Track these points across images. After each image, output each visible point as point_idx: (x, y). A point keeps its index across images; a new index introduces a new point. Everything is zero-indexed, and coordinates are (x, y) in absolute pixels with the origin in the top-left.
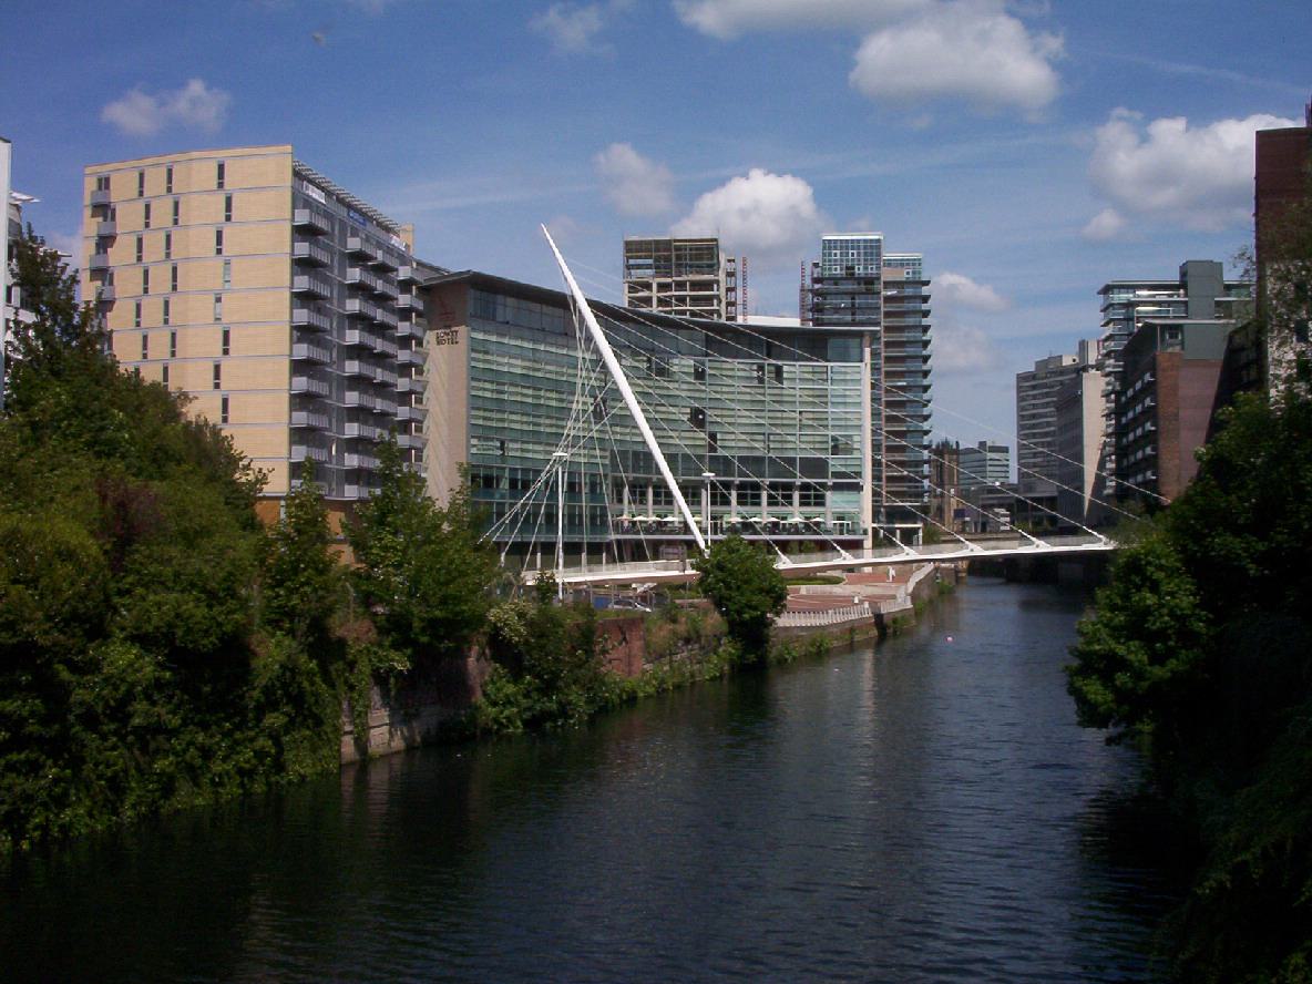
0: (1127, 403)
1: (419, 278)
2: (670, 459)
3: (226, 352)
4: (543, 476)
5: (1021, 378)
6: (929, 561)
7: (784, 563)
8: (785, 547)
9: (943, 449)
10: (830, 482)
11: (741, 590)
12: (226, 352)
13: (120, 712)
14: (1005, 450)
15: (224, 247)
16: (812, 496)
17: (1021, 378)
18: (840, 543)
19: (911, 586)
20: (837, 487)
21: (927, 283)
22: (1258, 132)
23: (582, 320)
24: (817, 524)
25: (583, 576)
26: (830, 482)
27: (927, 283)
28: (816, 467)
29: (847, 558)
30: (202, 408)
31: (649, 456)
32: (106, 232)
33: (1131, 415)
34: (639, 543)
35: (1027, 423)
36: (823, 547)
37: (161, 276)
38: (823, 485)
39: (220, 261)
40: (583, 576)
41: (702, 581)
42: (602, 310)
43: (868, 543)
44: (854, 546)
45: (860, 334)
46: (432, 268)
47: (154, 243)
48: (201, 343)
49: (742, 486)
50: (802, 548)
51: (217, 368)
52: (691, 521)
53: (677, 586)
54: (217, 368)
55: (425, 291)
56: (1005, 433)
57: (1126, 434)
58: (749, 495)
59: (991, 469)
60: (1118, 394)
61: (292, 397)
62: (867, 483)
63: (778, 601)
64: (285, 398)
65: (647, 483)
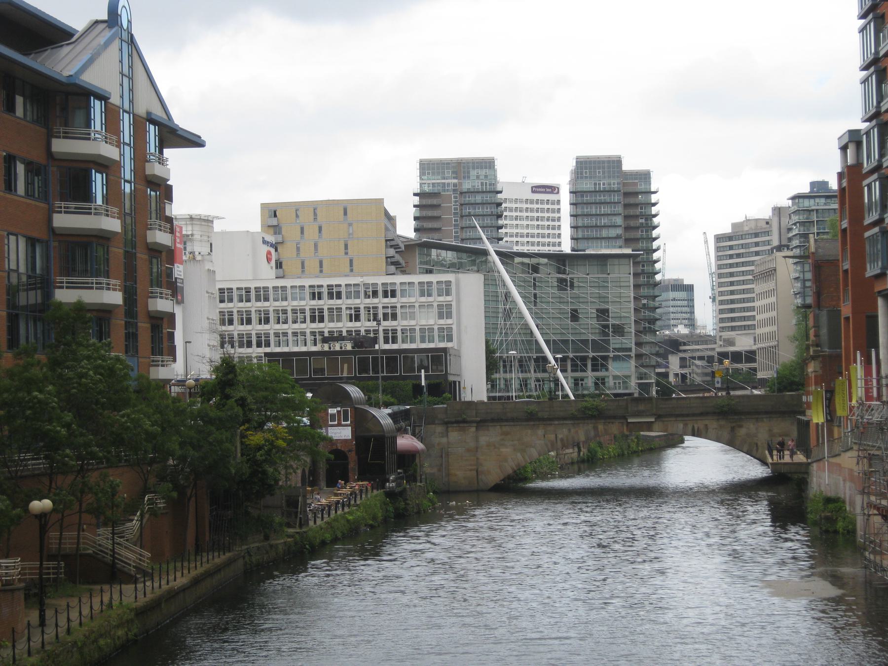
5: (719, 238)
10: (611, 355)
20: (616, 358)
22: (264, 206)
26: (611, 355)
38: (605, 358)
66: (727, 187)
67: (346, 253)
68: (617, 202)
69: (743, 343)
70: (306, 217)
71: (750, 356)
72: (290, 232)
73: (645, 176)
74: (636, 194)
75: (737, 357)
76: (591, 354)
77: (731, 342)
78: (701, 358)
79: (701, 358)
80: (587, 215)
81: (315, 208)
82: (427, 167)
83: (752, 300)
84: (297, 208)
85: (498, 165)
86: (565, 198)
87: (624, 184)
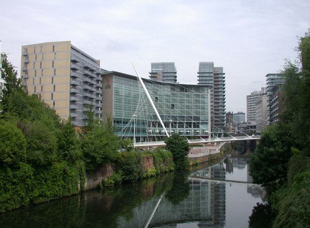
0: (272, 103)
1: (101, 73)
2: (162, 117)
3: (54, 90)
4: (131, 121)
5: (248, 96)
6: (224, 141)
7: (189, 142)
8: (190, 138)
9: (229, 114)
11: (177, 148)
12: (54, 90)
13: (23, 181)
14: (244, 114)
15: (55, 49)
16: (196, 126)
17: (248, 96)
18: (202, 137)
19: (220, 147)
20: (202, 123)
21: (224, 74)
23: (140, 83)
24: (197, 132)
25: (140, 145)
27: (224, 74)
28: (197, 118)
29: (204, 141)
30: (48, 102)
31: (156, 116)
32: (27, 61)
33: (273, 106)
34: (154, 137)
35: (249, 107)
36: (199, 138)
37: (39, 72)
38: (199, 123)
39: (53, 54)
40: (140, 145)
41: (167, 146)
42: (143, 79)
43: (210, 137)
44: (206, 137)
45: (208, 86)
46: (104, 70)
47: (38, 64)
48: (48, 88)
49: (179, 123)
50: (195, 138)
51: (52, 94)
52: (166, 131)
53: (162, 147)
54: (52, 94)
55: (103, 76)
56: (244, 109)
57: (272, 110)
58: (181, 125)
59: (211, 82)
60: (271, 100)
61: (70, 109)
62: (210, 123)
63: (187, 149)
64: (68, 110)
65: (156, 122)
66: (250, 71)
67: (53, 66)
68: (213, 80)
69: (253, 123)
70: (38, 50)
71: (255, 127)
72: (31, 58)
73: (221, 69)
74: (218, 74)
75: (251, 127)
76: (193, 122)
77: (250, 123)
78: (243, 128)
79: (243, 128)
80: (203, 80)
81: (41, 46)
82: (154, 65)
83: (255, 110)
84: (35, 47)
85: (176, 65)
86: (246, 115)
87: (215, 71)
